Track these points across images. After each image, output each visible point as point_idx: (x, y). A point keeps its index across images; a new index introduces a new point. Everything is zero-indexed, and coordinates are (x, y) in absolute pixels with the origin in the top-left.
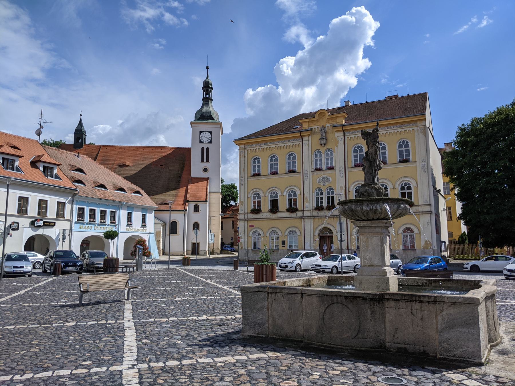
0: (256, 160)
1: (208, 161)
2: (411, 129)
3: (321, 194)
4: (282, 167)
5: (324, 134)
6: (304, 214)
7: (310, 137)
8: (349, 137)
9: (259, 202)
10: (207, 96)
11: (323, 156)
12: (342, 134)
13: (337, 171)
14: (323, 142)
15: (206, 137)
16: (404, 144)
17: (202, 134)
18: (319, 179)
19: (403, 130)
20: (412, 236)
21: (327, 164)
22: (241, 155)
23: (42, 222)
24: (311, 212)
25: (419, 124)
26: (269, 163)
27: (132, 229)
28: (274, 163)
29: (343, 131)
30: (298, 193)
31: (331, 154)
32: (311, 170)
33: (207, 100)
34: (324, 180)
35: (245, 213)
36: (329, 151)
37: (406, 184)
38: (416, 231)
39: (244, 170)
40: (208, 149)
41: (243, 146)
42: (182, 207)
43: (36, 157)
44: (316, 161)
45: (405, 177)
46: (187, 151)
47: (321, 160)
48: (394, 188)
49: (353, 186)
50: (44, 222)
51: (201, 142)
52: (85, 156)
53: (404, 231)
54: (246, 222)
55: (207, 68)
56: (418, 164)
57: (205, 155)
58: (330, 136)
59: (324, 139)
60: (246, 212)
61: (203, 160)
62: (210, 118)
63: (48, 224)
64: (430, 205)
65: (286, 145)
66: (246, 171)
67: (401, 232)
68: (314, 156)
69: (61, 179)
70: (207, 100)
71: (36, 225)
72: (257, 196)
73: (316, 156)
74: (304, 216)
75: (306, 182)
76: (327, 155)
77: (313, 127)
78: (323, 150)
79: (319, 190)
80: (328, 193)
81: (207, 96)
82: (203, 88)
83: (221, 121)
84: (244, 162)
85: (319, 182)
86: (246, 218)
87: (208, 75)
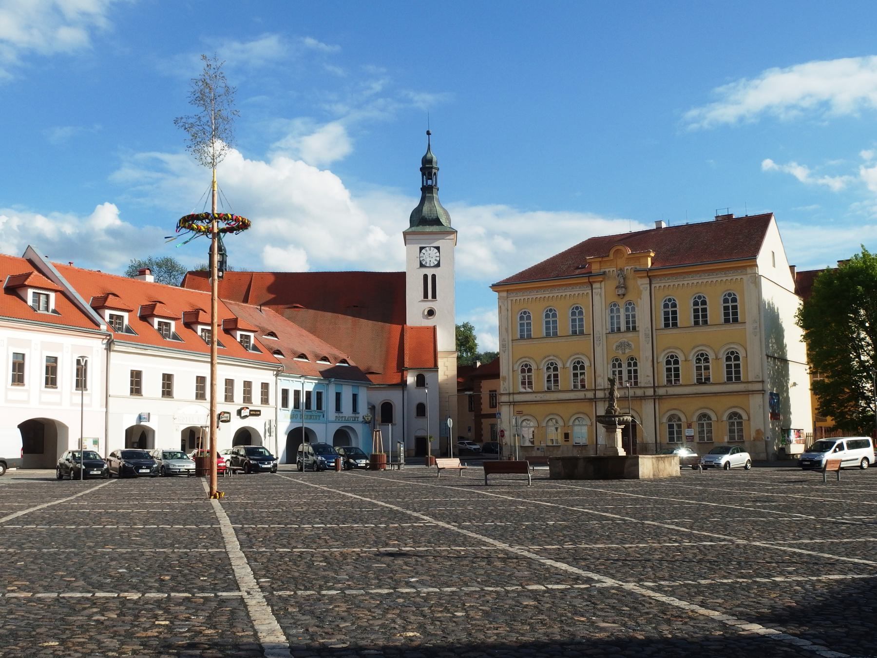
0: (525, 316)
1: (434, 296)
2: (739, 277)
3: (620, 366)
4: (564, 325)
5: (622, 281)
6: (655, 391)
7: (603, 283)
8: (657, 285)
9: (677, 369)
10: (430, 182)
11: (622, 311)
12: (647, 281)
13: (641, 334)
14: (621, 291)
15: (430, 256)
16: (577, 311)
17: (423, 251)
18: (617, 344)
19: (729, 278)
20: (740, 424)
21: (628, 323)
24: (645, 390)
25: (749, 270)
26: (544, 320)
28: (551, 319)
29: (649, 277)
30: (586, 364)
31: (633, 309)
32: (604, 332)
34: (623, 346)
35: (509, 394)
36: (630, 304)
37: (732, 353)
38: (745, 417)
40: (434, 277)
41: (504, 294)
42: (396, 380)
43: (13, 278)
44: (612, 318)
45: (733, 343)
46: (399, 279)
47: (618, 317)
48: (717, 359)
49: (663, 355)
51: (422, 266)
53: (730, 417)
54: (512, 406)
55: (428, 133)
56: (747, 326)
57: (430, 287)
58: (630, 283)
59: (623, 288)
62: (437, 222)
64: (763, 382)
65: (568, 294)
67: (725, 417)
68: (608, 311)
70: (428, 191)
72: (672, 361)
73: (612, 311)
74: (595, 398)
75: (598, 349)
76: (627, 310)
77: (607, 270)
78: (622, 303)
79: (617, 360)
80: (629, 365)
81: (430, 182)
82: (421, 169)
83: (454, 225)
85: (617, 347)
86: (511, 400)
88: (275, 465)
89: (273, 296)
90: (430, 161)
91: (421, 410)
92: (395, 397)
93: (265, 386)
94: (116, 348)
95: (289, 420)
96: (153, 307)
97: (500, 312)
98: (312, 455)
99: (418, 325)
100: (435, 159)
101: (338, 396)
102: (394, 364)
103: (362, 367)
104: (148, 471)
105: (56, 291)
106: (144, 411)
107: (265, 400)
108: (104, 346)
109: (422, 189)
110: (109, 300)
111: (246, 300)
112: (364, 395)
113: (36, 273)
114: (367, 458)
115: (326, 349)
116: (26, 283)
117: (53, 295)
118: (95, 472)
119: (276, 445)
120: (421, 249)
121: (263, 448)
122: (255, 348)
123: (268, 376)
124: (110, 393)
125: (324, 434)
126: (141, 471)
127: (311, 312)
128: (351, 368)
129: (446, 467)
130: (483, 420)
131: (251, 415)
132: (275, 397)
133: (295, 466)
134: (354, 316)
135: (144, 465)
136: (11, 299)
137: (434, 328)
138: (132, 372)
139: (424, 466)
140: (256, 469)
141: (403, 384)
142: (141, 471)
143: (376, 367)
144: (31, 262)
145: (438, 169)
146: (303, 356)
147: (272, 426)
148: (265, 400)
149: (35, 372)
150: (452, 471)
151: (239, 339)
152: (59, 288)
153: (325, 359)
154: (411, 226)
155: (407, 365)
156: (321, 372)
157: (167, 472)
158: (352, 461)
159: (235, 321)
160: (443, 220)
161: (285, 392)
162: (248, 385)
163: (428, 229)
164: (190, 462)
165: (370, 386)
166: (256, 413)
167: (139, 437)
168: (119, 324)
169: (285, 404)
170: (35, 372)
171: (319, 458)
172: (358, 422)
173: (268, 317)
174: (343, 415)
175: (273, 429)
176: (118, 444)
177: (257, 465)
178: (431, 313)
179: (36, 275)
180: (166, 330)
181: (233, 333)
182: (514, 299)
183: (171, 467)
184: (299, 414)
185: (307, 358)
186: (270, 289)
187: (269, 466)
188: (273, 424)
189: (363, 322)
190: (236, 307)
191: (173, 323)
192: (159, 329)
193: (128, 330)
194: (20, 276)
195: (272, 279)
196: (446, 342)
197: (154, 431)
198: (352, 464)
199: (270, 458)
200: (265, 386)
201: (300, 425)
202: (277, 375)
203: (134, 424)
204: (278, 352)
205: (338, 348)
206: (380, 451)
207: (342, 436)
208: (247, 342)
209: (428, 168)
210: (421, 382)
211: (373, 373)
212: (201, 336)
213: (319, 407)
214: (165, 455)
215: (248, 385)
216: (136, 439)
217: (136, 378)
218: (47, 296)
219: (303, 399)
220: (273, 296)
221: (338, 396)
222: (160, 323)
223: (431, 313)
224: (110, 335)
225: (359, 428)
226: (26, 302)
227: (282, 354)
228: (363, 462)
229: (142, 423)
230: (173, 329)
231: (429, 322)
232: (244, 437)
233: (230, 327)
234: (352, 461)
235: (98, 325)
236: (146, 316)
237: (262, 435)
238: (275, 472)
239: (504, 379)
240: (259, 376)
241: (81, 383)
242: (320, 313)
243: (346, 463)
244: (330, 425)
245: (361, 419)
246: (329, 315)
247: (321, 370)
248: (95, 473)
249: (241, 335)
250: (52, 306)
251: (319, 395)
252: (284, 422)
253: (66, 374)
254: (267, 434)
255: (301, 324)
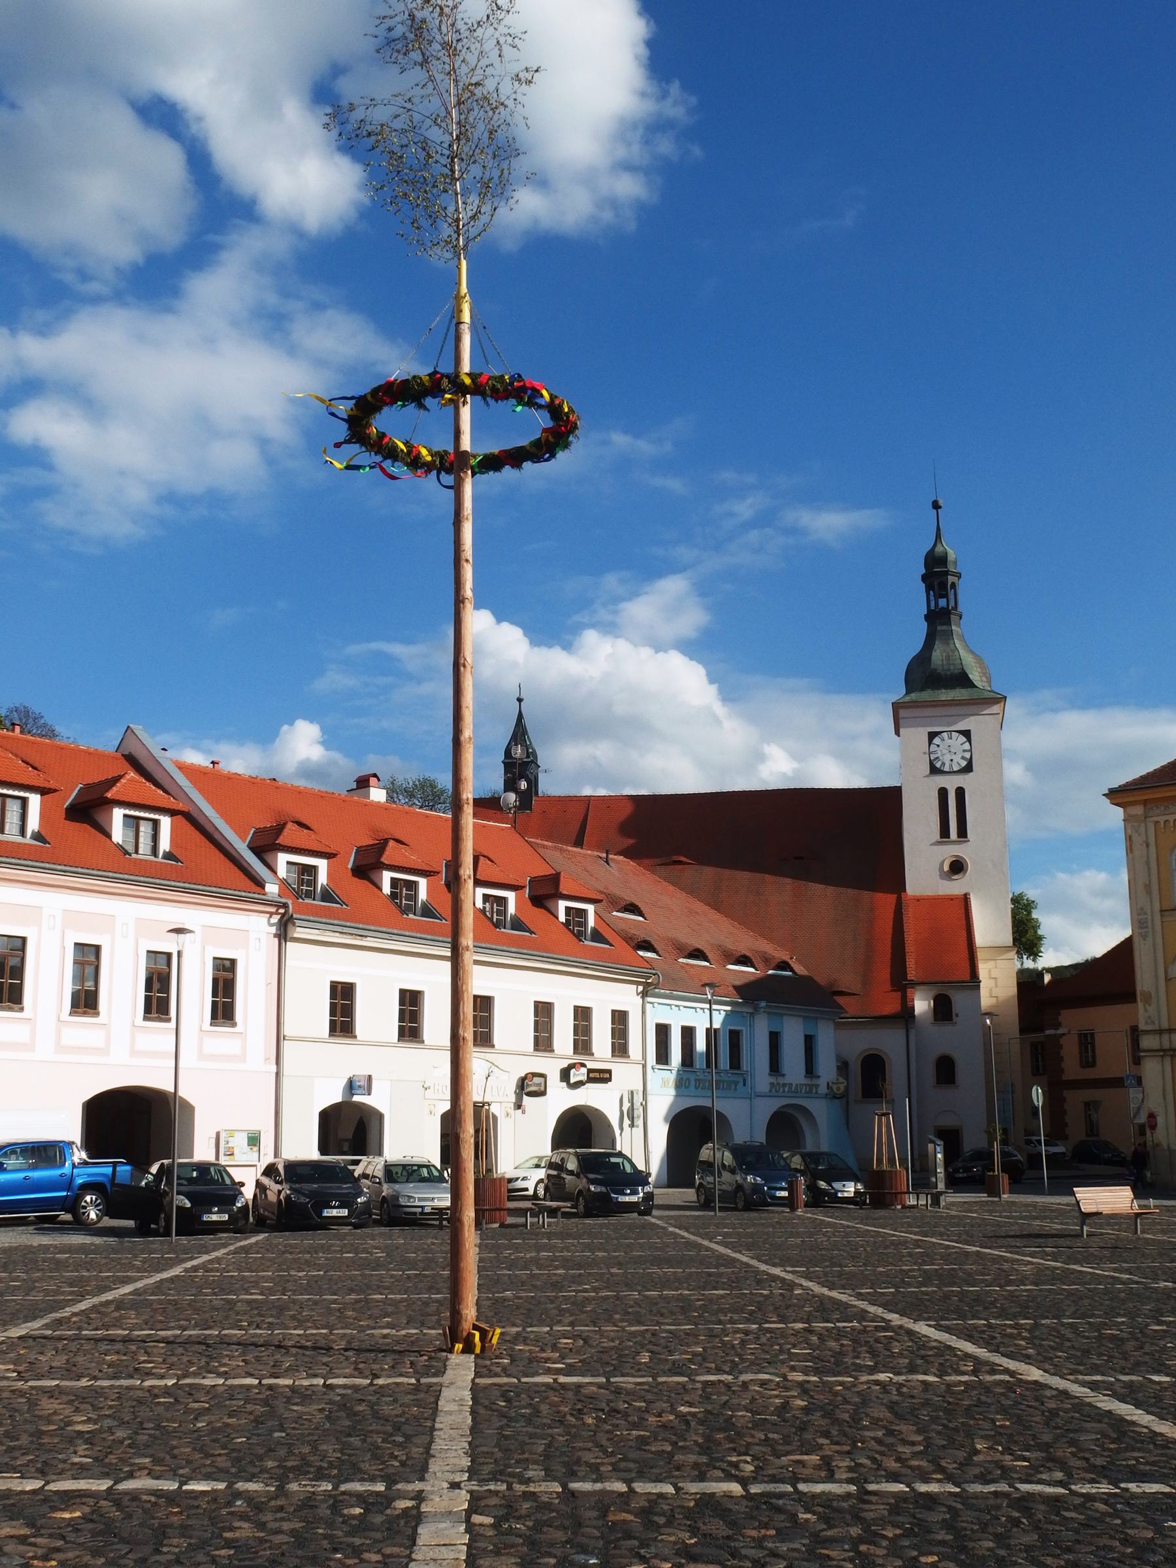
1: (962, 832)
10: (942, 602)
15: (952, 750)
17: (937, 740)
22: (1135, 838)
23: (584, 1070)
27: (784, 1085)
33: (940, 619)
35: (1160, 1032)
39: (1148, 888)
40: (960, 793)
41: (1138, 810)
42: (891, 1006)
43: (88, 788)
50: (590, 1071)
51: (934, 770)
52: (621, 858)
54: (1168, 1060)
55: (936, 506)
57: (953, 816)
60: (1165, 1025)
61: (945, 832)
62: (962, 680)
63: (597, 1075)
66: (1155, 893)
69: (611, 945)
70: (940, 619)
71: (572, 1081)
81: (942, 602)
82: (924, 578)
84: (1148, 863)
86: (1166, 1045)
87: (938, 529)
88: (649, 1197)
89: (631, 841)
90: (943, 560)
91: (946, 1070)
92: (889, 1042)
93: (620, 1019)
94: (299, 932)
95: (672, 1092)
96: (381, 846)
97: (1130, 849)
98: (732, 1171)
99: (929, 892)
100: (952, 555)
101: (775, 1040)
102: (883, 973)
103: (821, 979)
104: (344, 1212)
105: (172, 813)
106: (360, 1070)
107: (620, 1048)
108: (273, 930)
109: (927, 618)
110: (286, 832)
111: (579, 843)
112: (827, 1039)
113: (132, 774)
114: (856, 1179)
115: (745, 942)
116: (109, 795)
117: (166, 822)
118: (215, 1217)
119: (645, 1146)
120: (932, 736)
121: (620, 1155)
122: (597, 936)
123: (626, 996)
124: (287, 1031)
125: (747, 1119)
126: (327, 1213)
127: (709, 871)
128: (798, 979)
129: (1106, 1209)
130: (1066, 1093)
131: (590, 1080)
132: (640, 1041)
133: (689, 1194)
134: (796, 877)
135: (335, 1196)
136: (79, 832)
137: (966, 899)
138: (334, 986)
139: (983, 1197)
140: (601, 1207)
141: (907, 1013)
142: (327, 1213)
143: (848, 980)
144: (133, 761)
145: (959, 576)
146: (698, 954)
147: (637, 1104)
148: (620, 1048)
149: (122, 986)
150: (1113, 1219)
151: (562, 917)
152: (180, 806)
153: (744, 960)
154: (908, 692)
155: (912, 974)
156: (736, 988)
157: (394, 1215)
158: (822, 1184)
159: (555, 879)
160: (975, 676)
161: (663, 1031)
162: (583, 1015)
163: (945, 695)
164: (444, 1191)
165: (842, 1022)
166: (601, 1077)
167: (350, 1125)
168: (309, 883)
169: (663, 1056)
170: (122, 986)
171: (750, 1178)
172: (817, 1096)
173: (622, 875)
174: (787, 1080)
175: (639, 1111)
176: (303, 1145)
177: (604, 1198)
178: (957, 867)
179: (131, 780)
180: (408, 897)
181: (549, 904)
182: (1162, 819)
183: (402, 1201)
184: (692, 1077)
185: (706, 959)
186: (626, 828)
187: (634, 1199)
188: (638, 1099)
189: (817, 888)
190: (557, 854)
191: (423, 883)
192: (394, 896)
193: (327, 896)
194: (100, 783)
195: (628, 809)
196: (990, 926)
197: (381, 1116)
198: (824, 1192)
199: (640, 1178)
200: (620, 1019)
201: (707, 1103)
202: (644, 994)
203: (339, 1100)
204: (647, 946)
205: (770, 939)
206: (891, 1161)
207: (785, 1126)
208: (580, 924)
209: (937, 575)
210: (943, 1009)
211: (841, 993)
212: (483, 911)
213: (735, 1062)
214: (393, 1173)
215: (583, 1015)
216: (347, 1131)
217: (342, 999)
218: (156, 824)
219: (701, 1045)
220: (631, 841)
221: (775, 1040)
222: (394, 882)
223: (957, 867)
224: (285, 906)
225: (820, 1109)
226: (109, 836)
227: (654, 950)
228: (849, 1189)
229: (356, 1098)
230: (423, 895)
231: (955, 888)
232: (578, 1128)
233: (544, 893)
234: (822, 1184)
235: (260, 884)
236: (366, 867)
237: (615, 1123)
238: (647, 1212)
239: (1147, 998)
240: (608, 996)
241: (223, 1010)
242: (727, 872)
243: (812, 1188)
244: (759, 1102)
245: (823, 1090)
246: (743, 876)
247: (738, 983)
248: (215, 1217)
249: (568, 909)
250: (165, 844)
251: (734, 1036)
252: (662, 1097)
253: (193, 991)
254: (627, 1122)
255: (691, 891)
